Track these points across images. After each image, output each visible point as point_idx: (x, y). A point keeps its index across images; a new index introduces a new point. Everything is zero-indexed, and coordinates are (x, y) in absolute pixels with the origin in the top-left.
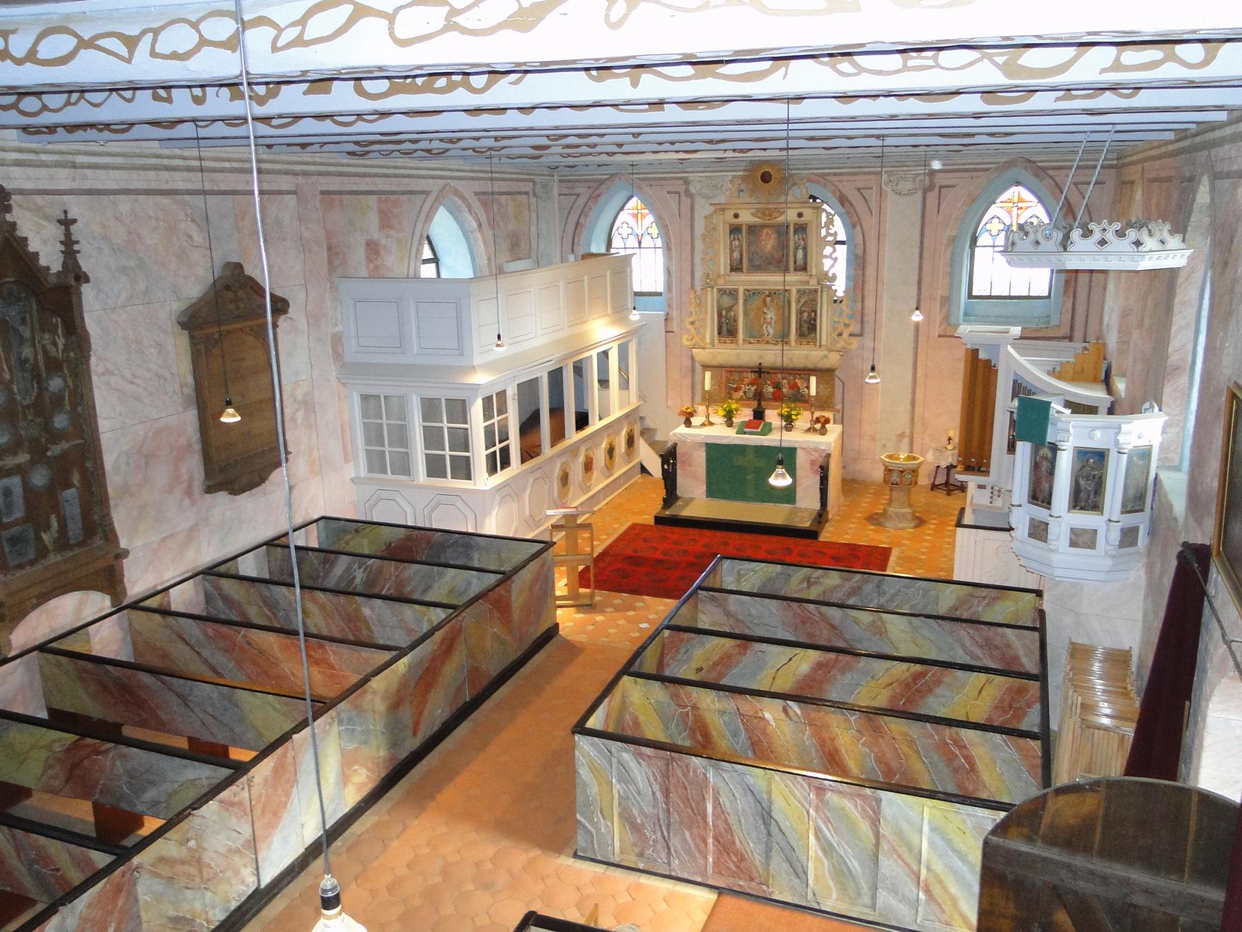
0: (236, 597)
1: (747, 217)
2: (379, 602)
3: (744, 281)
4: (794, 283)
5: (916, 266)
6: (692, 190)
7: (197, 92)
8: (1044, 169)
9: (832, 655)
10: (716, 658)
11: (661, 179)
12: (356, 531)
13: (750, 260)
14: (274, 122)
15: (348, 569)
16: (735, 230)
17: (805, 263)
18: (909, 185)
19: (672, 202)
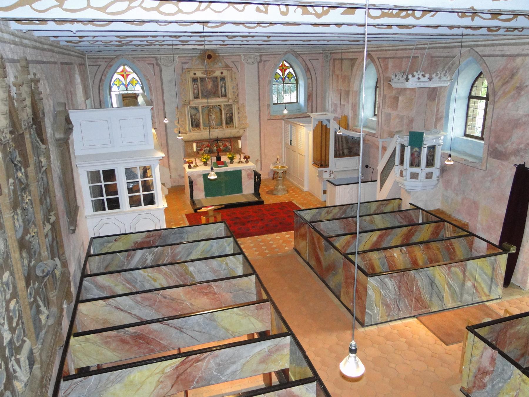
0: (107, 284)
1: (199, 75)
2: (164, 267)
3: (201, 102)
4: (222, 102)
5: (257, 93)
6: (159, 63)
7: (283, 8)
8: (298, 54)
9: (384, 231)
10: (344, 244)
11: (144, 58)
12: (115, 240)
13: (202, 93)
14: (209, 25)
15: (143, 255)
16: (195, 80)
17: (226, 94)
18: (252, 60)
19: (150, 67)
